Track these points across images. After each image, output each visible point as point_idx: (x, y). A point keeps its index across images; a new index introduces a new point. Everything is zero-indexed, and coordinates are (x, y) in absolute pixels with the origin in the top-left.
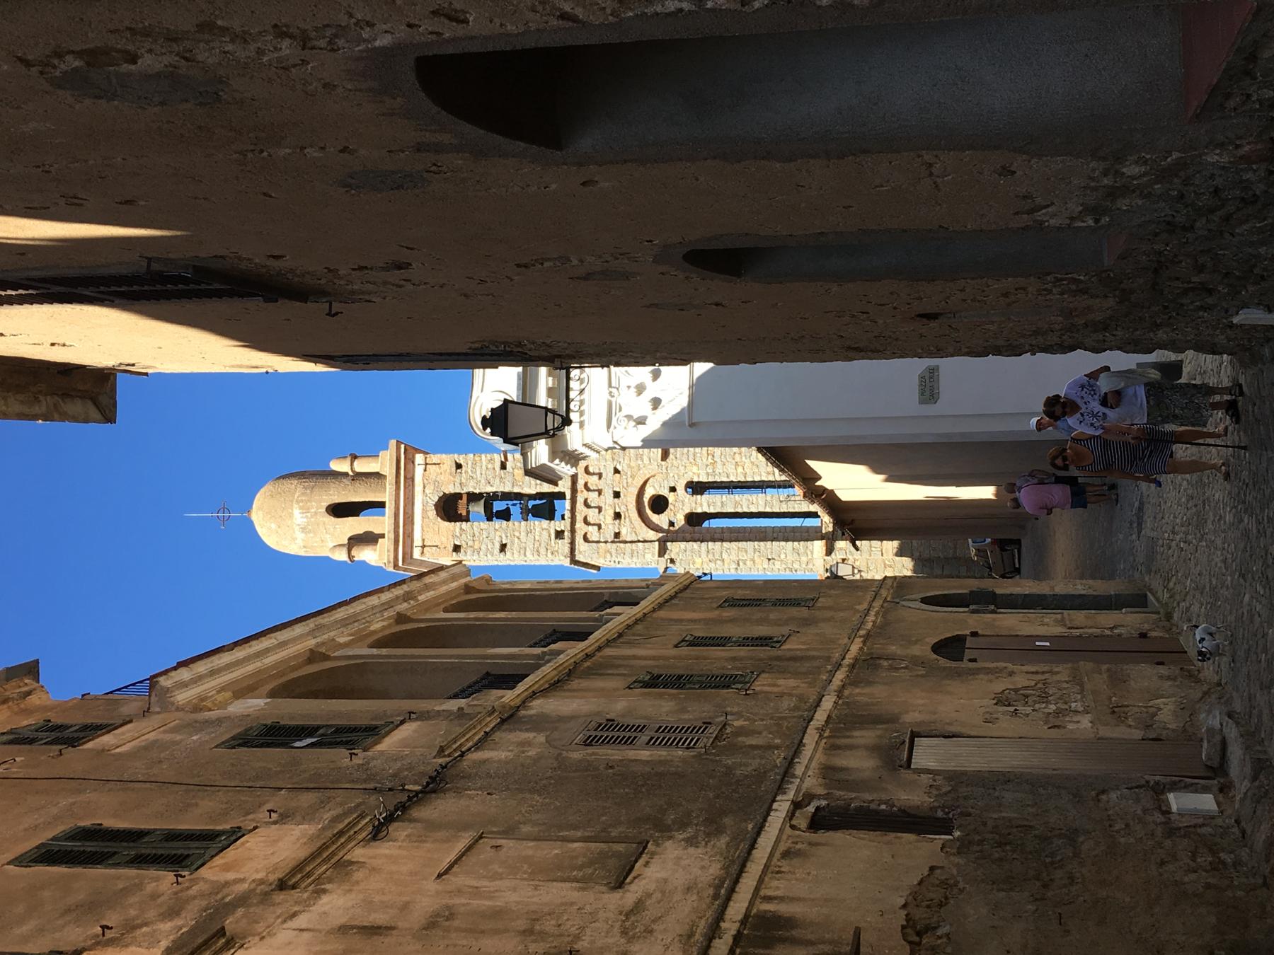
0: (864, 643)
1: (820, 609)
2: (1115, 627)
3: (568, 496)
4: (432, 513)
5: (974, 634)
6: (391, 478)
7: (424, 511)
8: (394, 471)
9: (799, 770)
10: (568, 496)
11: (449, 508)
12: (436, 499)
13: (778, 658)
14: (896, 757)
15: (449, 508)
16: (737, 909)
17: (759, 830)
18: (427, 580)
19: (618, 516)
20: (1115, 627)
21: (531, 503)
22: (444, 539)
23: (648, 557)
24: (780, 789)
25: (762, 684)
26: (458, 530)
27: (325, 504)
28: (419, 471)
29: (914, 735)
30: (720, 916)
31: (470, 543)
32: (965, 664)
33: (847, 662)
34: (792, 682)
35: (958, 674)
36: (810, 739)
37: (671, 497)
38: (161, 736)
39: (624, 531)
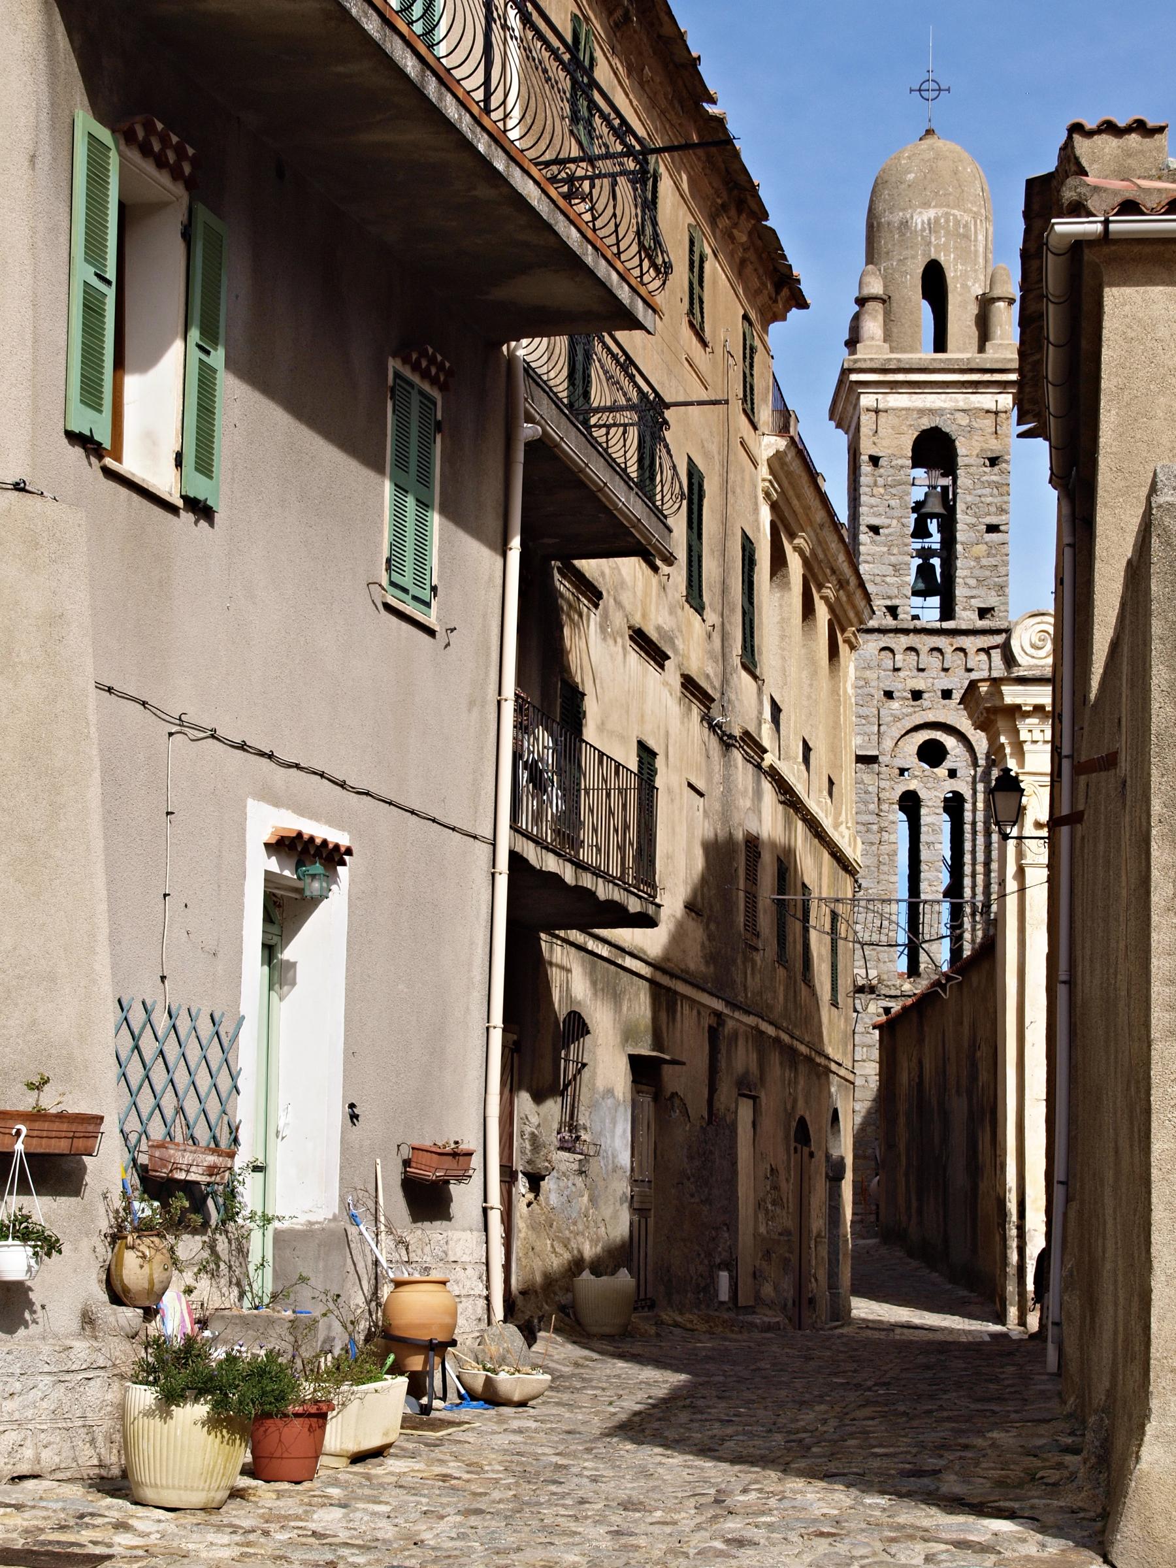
0: (806, 1056)
1: (830, 1010)
2: (816, 1280)
3: (947, 625)
4: (926, 423)
5: (811, 1155)
6: (980, 360)
7: (932, 412)
8: (988, 366)
9: (737, 1015)
10: (947, 625)
11: (934, 449)
12: (946, 429)
13: (795, 982)
14: (747, 1088)
15: (934, 449)
16: (681, 987)
17: (711, 994)
18: (858, 594)
19: (917, 695)
20: (816, 1280)
21: (936, 561)
22: (885, 443)
23: (859, 740)
24: (728, 1003)
25: (781, 972)
26: (900, 462)
27: (942, 259)
28: (986, 400)
29: (754, 1098)
30: (677, 977)
31: (880, 481)
32: (793, 1144)
33: (795, 1042)
34: (781, 998)
35: (787, 1137)
36: (751, 1020)
37: (942, 771)
38: (848, 812)
39: (895, 705)
